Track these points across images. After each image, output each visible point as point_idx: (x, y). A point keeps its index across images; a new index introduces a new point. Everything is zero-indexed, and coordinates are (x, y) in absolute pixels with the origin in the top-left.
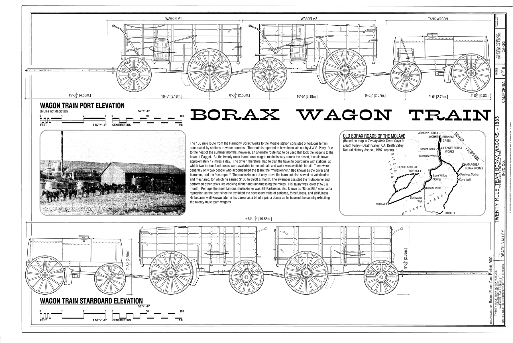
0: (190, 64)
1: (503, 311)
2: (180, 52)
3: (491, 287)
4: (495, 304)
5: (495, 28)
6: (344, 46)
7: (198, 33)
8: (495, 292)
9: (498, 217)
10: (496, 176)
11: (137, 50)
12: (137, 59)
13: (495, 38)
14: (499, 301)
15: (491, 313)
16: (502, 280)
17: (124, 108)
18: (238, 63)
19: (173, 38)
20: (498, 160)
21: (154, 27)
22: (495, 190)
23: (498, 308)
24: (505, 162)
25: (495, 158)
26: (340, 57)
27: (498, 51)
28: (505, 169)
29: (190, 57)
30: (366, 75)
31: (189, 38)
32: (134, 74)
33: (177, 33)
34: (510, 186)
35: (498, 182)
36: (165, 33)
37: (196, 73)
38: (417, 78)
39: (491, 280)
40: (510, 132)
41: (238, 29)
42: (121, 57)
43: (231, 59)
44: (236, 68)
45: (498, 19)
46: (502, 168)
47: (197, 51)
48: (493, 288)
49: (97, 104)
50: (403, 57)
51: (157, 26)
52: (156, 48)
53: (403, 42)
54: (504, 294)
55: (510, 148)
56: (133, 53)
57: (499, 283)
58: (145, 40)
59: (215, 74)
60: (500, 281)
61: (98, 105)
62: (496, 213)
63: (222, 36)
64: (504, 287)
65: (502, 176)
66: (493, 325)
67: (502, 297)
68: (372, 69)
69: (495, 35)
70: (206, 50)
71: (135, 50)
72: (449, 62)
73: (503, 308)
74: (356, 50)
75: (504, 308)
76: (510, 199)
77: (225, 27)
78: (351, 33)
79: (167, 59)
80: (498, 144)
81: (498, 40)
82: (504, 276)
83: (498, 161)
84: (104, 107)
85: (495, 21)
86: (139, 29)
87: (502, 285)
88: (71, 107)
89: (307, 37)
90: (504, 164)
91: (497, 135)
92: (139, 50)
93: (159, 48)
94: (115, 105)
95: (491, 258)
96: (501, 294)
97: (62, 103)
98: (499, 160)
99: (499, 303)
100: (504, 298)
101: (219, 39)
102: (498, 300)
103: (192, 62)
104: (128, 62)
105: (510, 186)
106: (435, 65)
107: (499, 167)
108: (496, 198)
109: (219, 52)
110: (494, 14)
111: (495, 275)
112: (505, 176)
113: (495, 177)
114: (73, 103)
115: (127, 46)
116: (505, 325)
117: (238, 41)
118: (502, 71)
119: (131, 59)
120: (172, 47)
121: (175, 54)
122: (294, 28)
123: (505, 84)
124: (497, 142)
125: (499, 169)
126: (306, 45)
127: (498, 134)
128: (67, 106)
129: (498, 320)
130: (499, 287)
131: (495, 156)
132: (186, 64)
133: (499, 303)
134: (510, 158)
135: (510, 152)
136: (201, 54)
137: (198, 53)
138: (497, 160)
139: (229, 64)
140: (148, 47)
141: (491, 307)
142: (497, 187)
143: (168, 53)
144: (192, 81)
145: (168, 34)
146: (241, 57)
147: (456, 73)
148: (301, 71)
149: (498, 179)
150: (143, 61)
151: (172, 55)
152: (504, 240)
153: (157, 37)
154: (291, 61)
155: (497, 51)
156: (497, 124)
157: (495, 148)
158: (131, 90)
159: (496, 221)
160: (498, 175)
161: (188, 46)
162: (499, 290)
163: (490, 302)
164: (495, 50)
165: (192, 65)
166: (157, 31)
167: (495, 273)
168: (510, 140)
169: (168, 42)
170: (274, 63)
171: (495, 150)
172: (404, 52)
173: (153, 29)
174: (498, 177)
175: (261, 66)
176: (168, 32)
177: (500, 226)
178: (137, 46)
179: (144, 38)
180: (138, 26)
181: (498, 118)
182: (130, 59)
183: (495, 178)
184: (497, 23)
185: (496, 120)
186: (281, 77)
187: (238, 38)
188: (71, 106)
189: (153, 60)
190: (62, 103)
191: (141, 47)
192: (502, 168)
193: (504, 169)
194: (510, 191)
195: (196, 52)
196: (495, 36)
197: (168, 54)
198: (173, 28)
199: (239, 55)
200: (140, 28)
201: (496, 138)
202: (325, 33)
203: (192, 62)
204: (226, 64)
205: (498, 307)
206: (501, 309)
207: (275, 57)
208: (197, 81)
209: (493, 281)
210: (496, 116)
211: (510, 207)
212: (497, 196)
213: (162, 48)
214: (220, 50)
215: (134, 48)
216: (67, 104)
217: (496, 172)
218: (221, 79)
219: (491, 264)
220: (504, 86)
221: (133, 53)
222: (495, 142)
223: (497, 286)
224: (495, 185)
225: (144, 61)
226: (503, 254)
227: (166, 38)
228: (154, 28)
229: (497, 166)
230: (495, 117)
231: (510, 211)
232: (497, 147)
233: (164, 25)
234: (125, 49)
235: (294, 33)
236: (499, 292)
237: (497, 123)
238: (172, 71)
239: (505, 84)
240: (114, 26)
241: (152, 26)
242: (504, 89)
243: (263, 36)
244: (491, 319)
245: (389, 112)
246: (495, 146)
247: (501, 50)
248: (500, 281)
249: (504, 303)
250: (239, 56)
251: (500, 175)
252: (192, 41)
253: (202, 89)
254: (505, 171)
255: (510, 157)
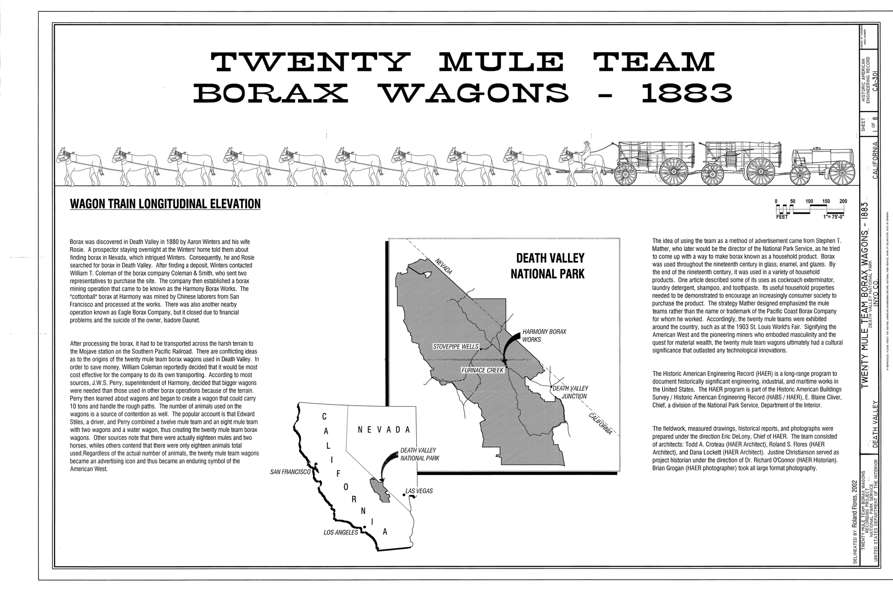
1: (875, 541)
2: (655, 160)
4: (861, 529)
5: (861, 48)
6: (760, 156)
8: (861, 508)
10: (862, 306)
13: (861, 67)
15: (855, 545)
16: (873, 487)
17: (134, 207)
18: (692, 167)
20: (866, 279)
22: (861, 331)
23: (867, 536)
24: (878, 283)
25: (862, 276)
26: (758, 163)
27: (865, 89)
28: (878, 294)
29: (661, 163)
30: (774, 175)
32: (626, 174)
35: (866, 316)
36: (645, 148)
37: (666, 173)
38: (808, 176)
40: (888, 230)
44: (691, 170)
45: (865, 33)
46: (872, 292)
49: (213, 201)
50: (798, 163)
53: (798, 154)
55: (887, 257)
56: (625, 161)
57: (869, 493)
59: (678, 175)
61: (214, 203)
62: (863, 371)
64: (877, 500)
65: (873, 307)
67: (874, 518)
68: (778, 170)
69: (861, 60)
72: (828, 166)
73: (876, 536)
74: (768, 159)
76: (888, 346)
78: (765, 148)
80: (866, 250)
81: (865, 70)
82: (877, 480)
83: (866, 281)
84: (225, 205)
85: (861, 36)
88: (123, 207)
89: (736, 150)
90: (877, 285)
91: (865, 235)
94: (244, 202)
95: (854, 483)
96: (873, 512)
97: (109, 200)
98: (868, 278)
99: (869, 527)
100: (877, 519)
101: (680, 152)
106: (819, 168)
107: (868, 290)
108: (862, 345)
109: (680, 160)
110: (859, 25)
111: (861, 479)
113: (862, 308)
114: (128, 200)
116: (878, 566)
118: (873, 124)
122: (728, 145)
124: (865, 247)
125: (869, 295)
126: (736, 155)
127: (866, 233)
128: (117, 205)
129: (868, 557)
130: (869, 499)
131: (861, 272)
132: (659, 168)
133: (869, 527)
135: (887, 265)
137: (667, 160)
138: (865, 278)
142: (864, 326)
147: (832, 173)
148: (733, 172)
149: (866, 312)
152: (878, 418)
154: (726, 166)
155: (863, 88)
156: (864, 217)
157: (862, 258)
159: (864, 384)
160: (866, 304)
161: (660, 156)
163: (854, 526)
164: (861, 86)
165: (663, 168)
167: (861, 475)
168: (887, 244)
170: (716, 167)
171: (862, 261)
172: (799, 160)
175: (707, 169)
177: (870, 393)
178: (627, 156)
180: (628, 143)
181: (865, 205)
183: (861, 309)
184: (863, 40)
185: (863, 210)
186: (720, 176)
188: (124, 205)
190: (109, 200)
192: (872, 292)
193: (876, 294)
194: (887, 332)
196: (861, 62)
201: (862, 240)
202: (748, 148)
204: (684, 168)
206: (873, 538)
207: (716, 163)
208: (666, 179)
210: (862, 202)
211: (888, 360)
212: (866, 341)
216: (117, 201)
217: (863, 299)
218: (681, 177)
220: (877, 150)
221: (625, 161)
222: (862, 247)
223: (866, 498)
224: (861, 322)
226: (876, 442)
229: (865, 289)
230: (861, 204)
231: (888, 366)
235: (728, 148)
238: (649, 172)
239: (878, 146)
242: (877, 155)
243: (708, 150)
244: (855, 556)
246: (861, 255)
247: (872, 87)
249: (877, 527)
250: (693, 163)
255: (887, 273)
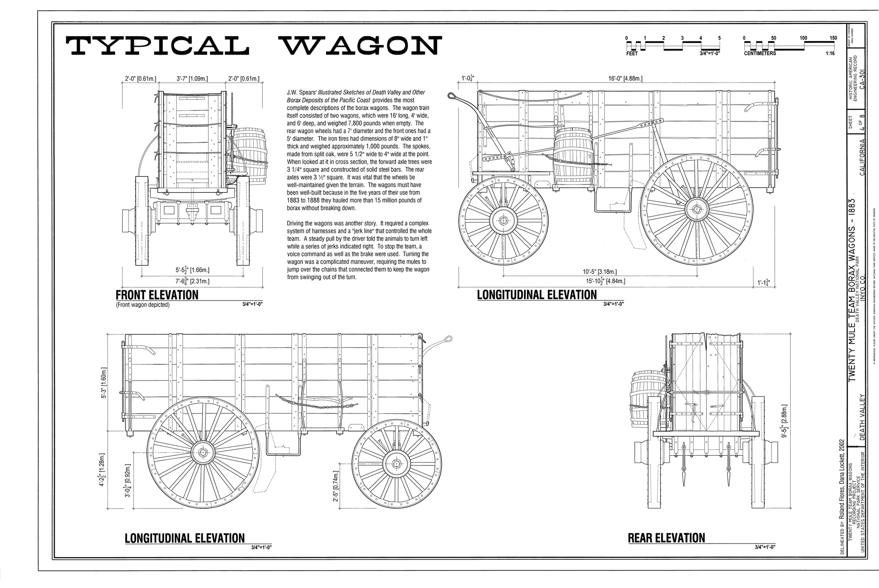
0: (647, 192)
1: (862, 533)
3: (842, 491)
4: (848, 521)
5: (848, 47)
7: (666, 113)
8: (848, 500)
9: (854, 372)
10: (849, 301)
11: (512, 158)
12: (511, 180)
13: (848, 65)
14: (856, 516)
15: (842, 536)
19: (601, 127)
21: (556, 97)
23: (854, 527)
24: (865, 278)
25: (849, 271)
27: (853, 87)
28: (865, 289)
29: (647, 176)
31: (644, 126)
33: (612, 113)
34: (874, 318)
35: (853, 311)
39: (842, 479)
41: (768, 104)
42: (469, 177)
43: (752, 180)
45: (852, 32)
47: (665, 161)
48: (845, 493)
51: (562, 95)
52: (561, 153)
54: (864, 503)
55: (874, 252)
56: (501, 165)
57: (856, 485)
58: (533, 132)
60: (858, 481)
62: (850, 365)
63: (729, 121)
65: (860, 302)
66: (846, 556)
67: (861, 509)
69: (848, 59)
70: (688, 157)
71: (507, 157)
73: (862, 527)
75: (864, 527)
77: (736, 98)
79: (588, 180)
80: (853, 246)
82: (864, 472)
83: (853, 276)
86: (517, 103)
87: (861, 489)
90: (864, 280)
91: (852, 231)
92: (516, 158)
93: (568, 153)
96: (860, 504)
98: (855, 273)
99: (856, 518)
100: (864, 510)
102: (854, 515)
103: (653, 189)
104: (489, 187)
105: (874, 318)
107: (855, 285)
108: (850, 340)
110: (847, 24)
111: (848, 471)
112: (865, 300)
113: (849, 303)
115: (486, 146)
116: (865, 557)
117: (770, 133)
118: (860, 122)
119: (497, 179)
120: (601, 150)
121: (608, 168)
123: (865, 144)
124: (853, 243)
125: (856, 290)
127: (853, 229)
129: (855, 548)
131: (849, 268)
132: (637, 194)
133: (856, 518)
134: (874, 270)
135: (874, 260)
136: (676, 168)
138: (852, 273)
139: (746, 193)
140: (539, 151)
141: (842, 526)
142: (852, 320)
143: (590, 164)
144: (652, 237)
145: (591, 116)
146: (777, 176)
149: (853, 307)
150: (525, 185)
151: (601, 171)
152: (864, 411)
153: (563, 123)
155: (851, 86)
156: (851, 213)
157: (849, 253)
158: (496, 261)
159: (851, 378)
160: (854, 299)
161: (642, 146)
162: (856, 497)
163: (841, 517)
164: (848, 85)
166: (562, 108)
167: (848, 467)
168: (874, 240)
169: (591, 137)
171: (849, 257)
173: (551, 103)
174: (853, 302)
176: (591, 111)
177: (857, 386)
178: (510, 146)
179: (528, 126)
180: (515, 95)
182: (494, 180)
184: (850, 39)
187: (770, 126)
189: (552, 183)
191: (522, 150)
192: (859, 287)
194: (874, 327)
195: (662, 164)
196: (848, 61)
197: (590, 166)
198: (602, 100)
199: (773, 169)
200: (519, 100)
201: (849, 236)
203: (653, 187)
204: (738, 194)
205: (856, 525)
206: (860, 530)
209: (845, 481)
210: (849, 198)
212: (853, 335)
213: (575, 152)
214: (725, 158)
215: (503, 153)
217: (850, 294)
219: (842, 452)
220: (864, 147)
221: (501, 165)
222: (849, 243)
223: (853, 490)
224: (848, 316)
225: (528, 187)
226: (863, 435)
227: (586, 126)
228: (556, 102)
230: (848, 201)
231: (874, 360)
232: (852, 252)
233: (581, 92)
234: (480, 154)
236: (856, 501)
237: (851, 211)
240: (451, 96)
241: (550, 96)
242: (864, 152)
244: (842, 547)
245: (106, 51)
247: (859, 85)
248: (858, 481)
249: (864, 518)
251: (857, 299)
252: (651, 135)
253: (678, 258)
254: (865, 293)
